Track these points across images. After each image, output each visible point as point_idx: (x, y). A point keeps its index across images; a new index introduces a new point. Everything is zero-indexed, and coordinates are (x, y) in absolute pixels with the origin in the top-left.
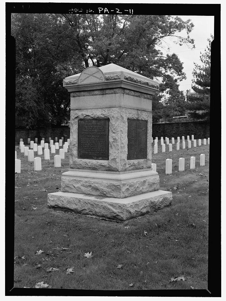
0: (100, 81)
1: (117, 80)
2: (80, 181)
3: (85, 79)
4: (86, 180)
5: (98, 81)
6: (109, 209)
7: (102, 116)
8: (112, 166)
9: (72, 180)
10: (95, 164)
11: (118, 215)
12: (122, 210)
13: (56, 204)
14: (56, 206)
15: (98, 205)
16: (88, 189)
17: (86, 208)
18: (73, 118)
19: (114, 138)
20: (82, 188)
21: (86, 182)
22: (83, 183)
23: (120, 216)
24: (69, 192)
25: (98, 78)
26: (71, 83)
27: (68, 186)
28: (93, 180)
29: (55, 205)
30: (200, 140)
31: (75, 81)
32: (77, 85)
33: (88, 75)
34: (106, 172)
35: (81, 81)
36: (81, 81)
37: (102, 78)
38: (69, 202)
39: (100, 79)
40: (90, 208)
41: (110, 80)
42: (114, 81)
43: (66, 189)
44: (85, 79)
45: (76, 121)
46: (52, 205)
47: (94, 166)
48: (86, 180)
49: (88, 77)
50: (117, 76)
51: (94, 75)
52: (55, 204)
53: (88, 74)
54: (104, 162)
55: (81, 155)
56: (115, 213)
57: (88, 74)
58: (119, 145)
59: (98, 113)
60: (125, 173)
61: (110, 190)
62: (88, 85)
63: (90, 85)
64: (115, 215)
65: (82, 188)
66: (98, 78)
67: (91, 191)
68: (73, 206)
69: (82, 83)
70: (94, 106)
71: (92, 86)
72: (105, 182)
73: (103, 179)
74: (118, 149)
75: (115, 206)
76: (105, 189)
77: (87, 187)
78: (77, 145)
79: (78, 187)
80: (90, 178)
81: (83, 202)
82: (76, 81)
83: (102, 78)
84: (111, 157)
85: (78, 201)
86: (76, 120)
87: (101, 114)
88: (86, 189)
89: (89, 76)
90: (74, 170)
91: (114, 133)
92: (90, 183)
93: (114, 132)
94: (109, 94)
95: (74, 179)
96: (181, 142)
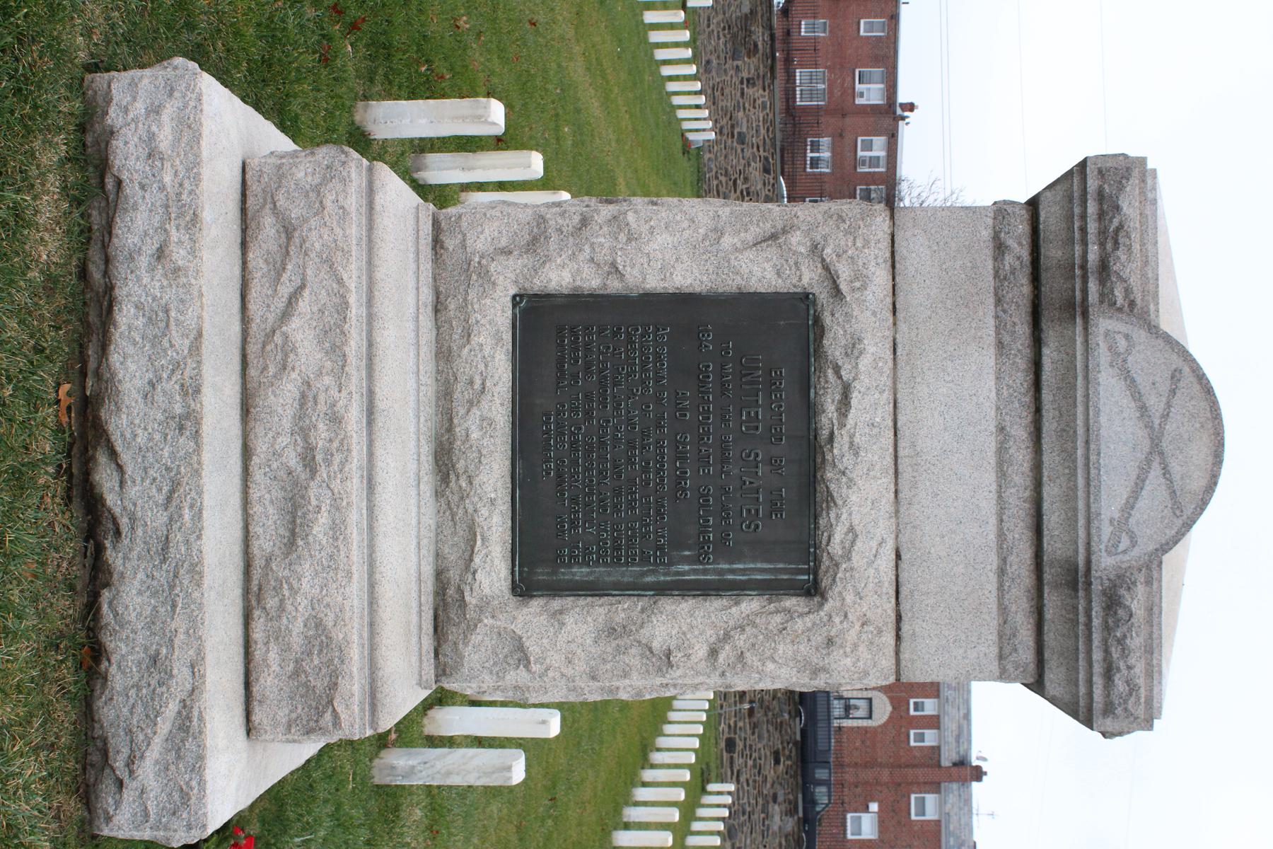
0: (1107, 530)
1: (1098, 681)
2: (336, 351)
3: (1131, 383)
4: (354, 417)
5: (1110, 505)
6: (152, 718)
7: (838, 536)
8: (475, 639)
9: (340, 282)
10: (476, 482)
11: (120, 784)
12: (160, 816)
13: (131, 190)
14: (110, 183)
15: (174, 606)
16: (284, 440)
17: (133, 491)
18: (828, 251)
19: (677, 657)
20: (289, 389)
21: (336, 420)
22: (322, 398)
23: (118, 804)
24: (244, 245)
25: (1129, 506)
26: (1109, 246)
27: (292, 250)
28: (356, 485)
29: (119, 183)
30: (710, 124)
31: (1128, 291)
32: (1093, 296)
33: (1155, 403)
34: (428, 570)
35: (1122, 344)
36: (1122, 344)
37: (1125, 542)
38: (160, 318)
39: (1122, 524)
40: (140, 532)
41: (1107, 628)
42: (1097, 655)
43: (268, 228)
44: (1131, 383)
45: (805, 280)
46: (118, 144)
47: (460, 466)
48: (354, 417)
49: (1143, 409)
50: (1133, 689)
51: (1156, 471)
52: (125, 176)
53: (1165, 416)
54: (493, 570)
55: (538, 318)
56: (130, 763)
57: (1165, 416)
58: (627, 682)
59: (860, 509)
60: (423, 442)
61: (296, 641)
62: (1080, 409)
63: (1080, 398)
64: (119, 764)
65: (289, 389)
66: (1129, 506)
67: (275, 466)
68: (133, 367)
69: (1102, 354)
70: (913, 445)
71: (1067, 433)
72: (356, 590)
73: (371, 573)
74: (594, 678)
75: (179, 757)
76: (299, 611)
77: (303, 430)
78: (614, 286)
79: (288, 349)
80: (371, 454)
81: (173, 456)
82: (1120, 302)
83: (1125, 542)
84: (531, 618)
85: (178, 409)
86: (809, 278)
87: (851, 529)
88: (287, 424)
89: (1149, 426)
90: (427, 267)
91: (713, 653)
92: (329, 454)
93: (722, 657)
94: (1001, 587)
95: (352, 299)
96: (686, 78)
